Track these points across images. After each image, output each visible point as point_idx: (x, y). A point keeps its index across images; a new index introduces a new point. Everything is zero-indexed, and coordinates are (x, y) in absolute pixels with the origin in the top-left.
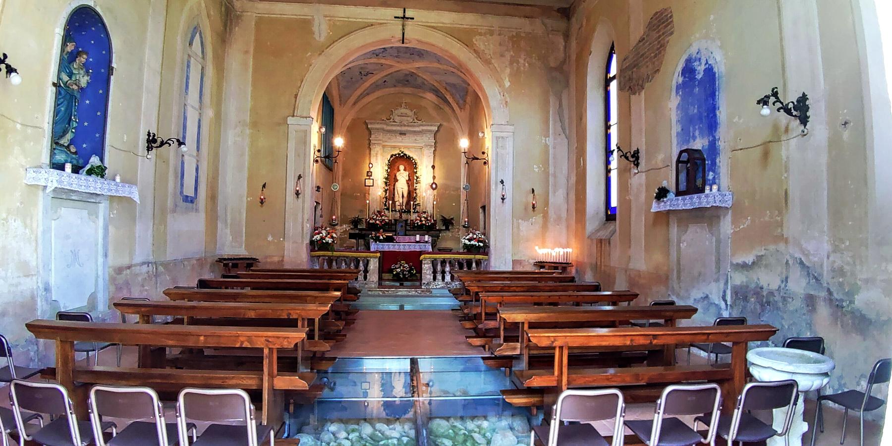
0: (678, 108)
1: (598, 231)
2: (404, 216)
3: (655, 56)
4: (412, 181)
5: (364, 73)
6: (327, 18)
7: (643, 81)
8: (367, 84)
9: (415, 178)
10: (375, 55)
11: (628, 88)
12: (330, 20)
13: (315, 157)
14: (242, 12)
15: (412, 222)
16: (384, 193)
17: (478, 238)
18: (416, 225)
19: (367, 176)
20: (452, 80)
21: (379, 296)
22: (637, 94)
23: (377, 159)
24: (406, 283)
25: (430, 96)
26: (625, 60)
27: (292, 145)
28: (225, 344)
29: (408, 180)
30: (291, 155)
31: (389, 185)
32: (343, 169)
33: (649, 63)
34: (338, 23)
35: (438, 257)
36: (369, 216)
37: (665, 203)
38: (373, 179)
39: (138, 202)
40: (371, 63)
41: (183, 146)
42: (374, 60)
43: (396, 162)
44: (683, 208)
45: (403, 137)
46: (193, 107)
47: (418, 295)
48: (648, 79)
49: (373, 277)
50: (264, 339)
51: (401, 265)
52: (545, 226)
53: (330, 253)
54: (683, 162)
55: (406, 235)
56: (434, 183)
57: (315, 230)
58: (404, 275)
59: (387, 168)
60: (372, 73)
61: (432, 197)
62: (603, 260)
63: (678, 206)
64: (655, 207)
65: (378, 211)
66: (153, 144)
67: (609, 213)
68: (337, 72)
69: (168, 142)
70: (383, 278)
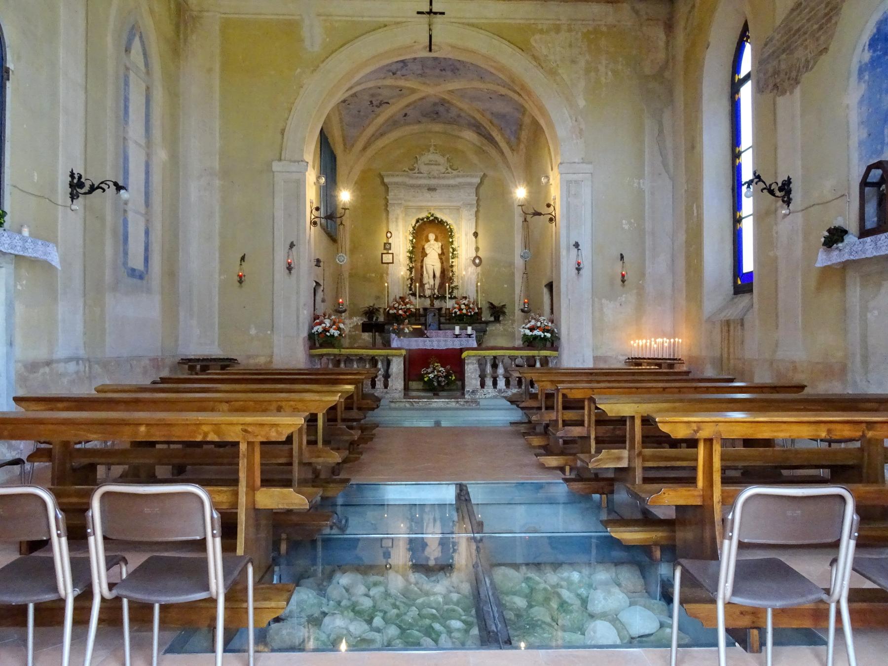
0: (861, 102)
1: (721, 310)
2: (437, 304)
3: (820, 28)
4: (446, 255)
5: (377, 103)
6: (322, 18)
7: (798, 71)
8: (380, 120)
9: (451, 250)
10: (391, 73)
11: (771, 87)
12: (325, 20)
13: (313, 217)
14: (200, 11)
15: (447, 311)
16: (408, 272)
17: (543, 326)
18: (453, 315)
19: (385, 249)
20: (500, 107)
21: (405, 409)
22: (788, 93)
23: (397, 226)
24: (441, 394)
25: (469, 135)
26: (766, 45)
27: (279, 201)
28: (178, 437)
29: (442, 254)
30: (279, 214)
31: (415, 261)
32: (352, 241)
33: (808, 41)
34: (337, 25)
35: (487, 354)
36: (388, 304)
37: (840, 250)
38: (393, 254)
39: (59, 268)
40: (387, 87)
41: (122, 191)
42: (389, 82)
43: (424, 230)
44: (875, 254)
45: (433, 193)
46: (136, 142)
47: (461, 406)
48: (807, 66)
49: (397, 383)
50: (240, 427)
51: (434, 369)
52: (640, 309)
53: (336, 351)
54: (872, 185)
55: (440, 329)
56: (477, 257)
57: (315, 320)
58: (439, 382)
59: (411, 238)
60: (388, 103)
61: (474, 277)
62: (731, 350)
63: (864, 253)
64: (823, 259)
65: (401, 298)
66: (79, 190)
67: (739, 282)
68: (340, 96)
69: (101, 185)
70: (410, 388)
